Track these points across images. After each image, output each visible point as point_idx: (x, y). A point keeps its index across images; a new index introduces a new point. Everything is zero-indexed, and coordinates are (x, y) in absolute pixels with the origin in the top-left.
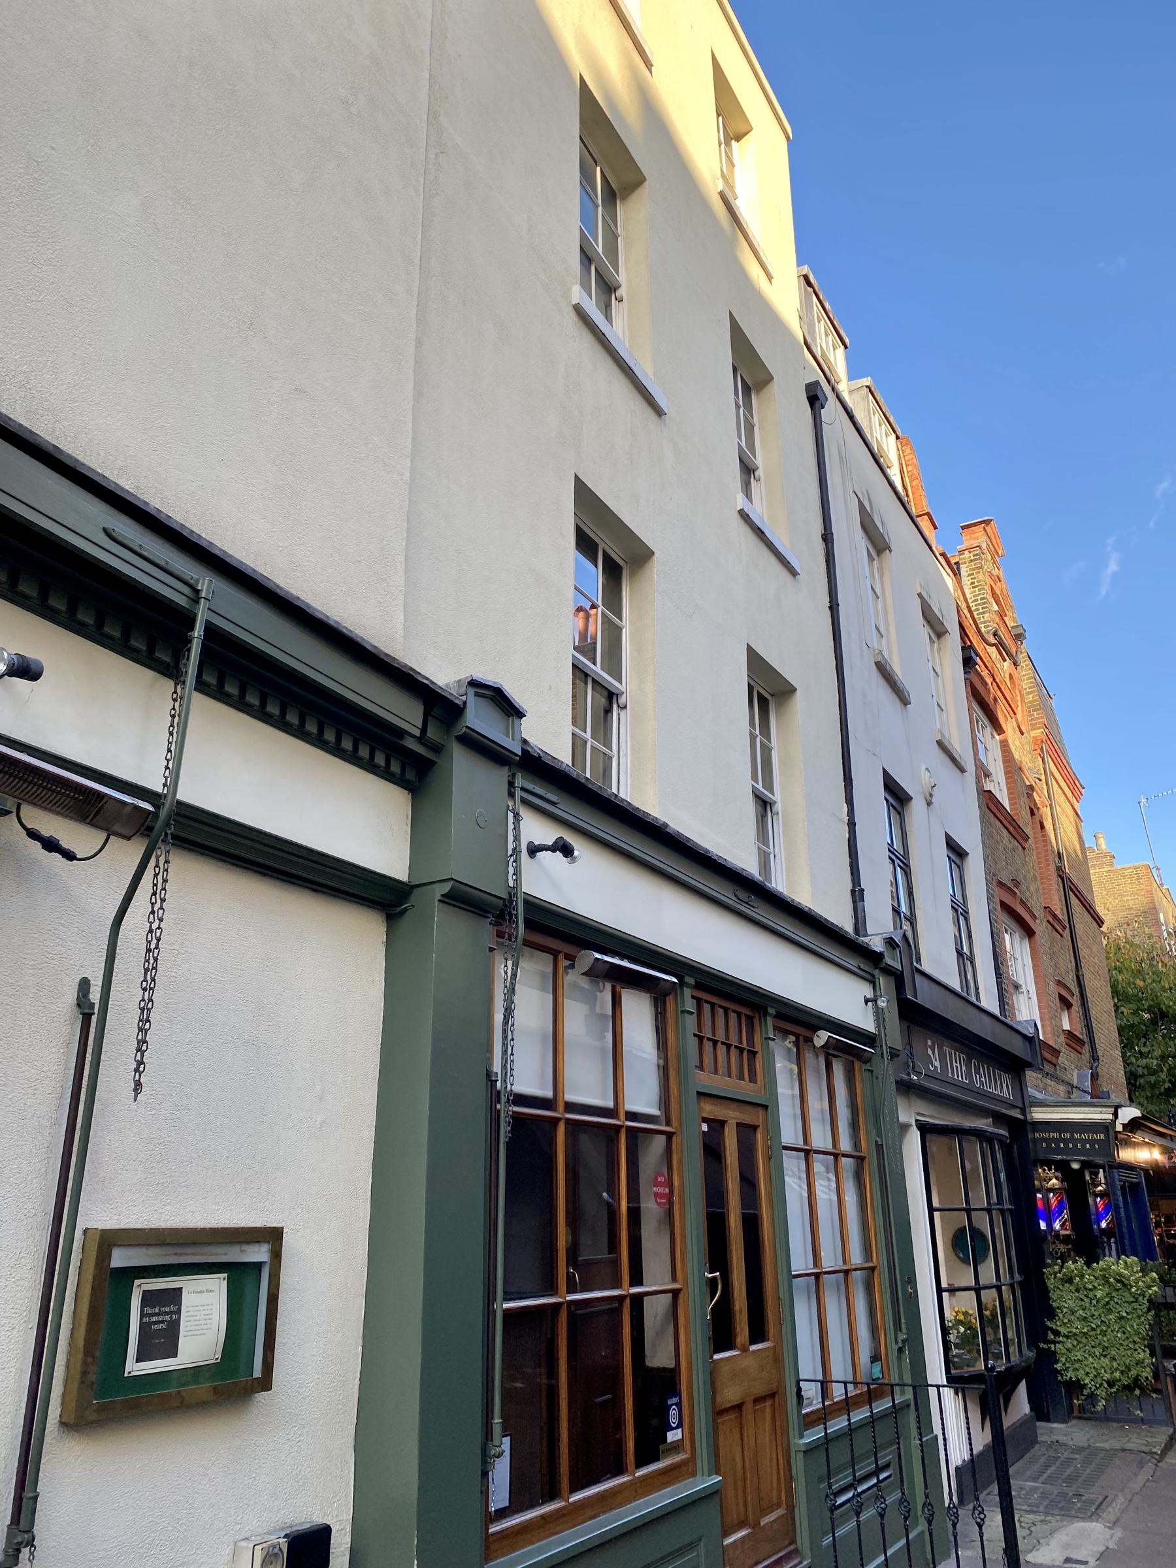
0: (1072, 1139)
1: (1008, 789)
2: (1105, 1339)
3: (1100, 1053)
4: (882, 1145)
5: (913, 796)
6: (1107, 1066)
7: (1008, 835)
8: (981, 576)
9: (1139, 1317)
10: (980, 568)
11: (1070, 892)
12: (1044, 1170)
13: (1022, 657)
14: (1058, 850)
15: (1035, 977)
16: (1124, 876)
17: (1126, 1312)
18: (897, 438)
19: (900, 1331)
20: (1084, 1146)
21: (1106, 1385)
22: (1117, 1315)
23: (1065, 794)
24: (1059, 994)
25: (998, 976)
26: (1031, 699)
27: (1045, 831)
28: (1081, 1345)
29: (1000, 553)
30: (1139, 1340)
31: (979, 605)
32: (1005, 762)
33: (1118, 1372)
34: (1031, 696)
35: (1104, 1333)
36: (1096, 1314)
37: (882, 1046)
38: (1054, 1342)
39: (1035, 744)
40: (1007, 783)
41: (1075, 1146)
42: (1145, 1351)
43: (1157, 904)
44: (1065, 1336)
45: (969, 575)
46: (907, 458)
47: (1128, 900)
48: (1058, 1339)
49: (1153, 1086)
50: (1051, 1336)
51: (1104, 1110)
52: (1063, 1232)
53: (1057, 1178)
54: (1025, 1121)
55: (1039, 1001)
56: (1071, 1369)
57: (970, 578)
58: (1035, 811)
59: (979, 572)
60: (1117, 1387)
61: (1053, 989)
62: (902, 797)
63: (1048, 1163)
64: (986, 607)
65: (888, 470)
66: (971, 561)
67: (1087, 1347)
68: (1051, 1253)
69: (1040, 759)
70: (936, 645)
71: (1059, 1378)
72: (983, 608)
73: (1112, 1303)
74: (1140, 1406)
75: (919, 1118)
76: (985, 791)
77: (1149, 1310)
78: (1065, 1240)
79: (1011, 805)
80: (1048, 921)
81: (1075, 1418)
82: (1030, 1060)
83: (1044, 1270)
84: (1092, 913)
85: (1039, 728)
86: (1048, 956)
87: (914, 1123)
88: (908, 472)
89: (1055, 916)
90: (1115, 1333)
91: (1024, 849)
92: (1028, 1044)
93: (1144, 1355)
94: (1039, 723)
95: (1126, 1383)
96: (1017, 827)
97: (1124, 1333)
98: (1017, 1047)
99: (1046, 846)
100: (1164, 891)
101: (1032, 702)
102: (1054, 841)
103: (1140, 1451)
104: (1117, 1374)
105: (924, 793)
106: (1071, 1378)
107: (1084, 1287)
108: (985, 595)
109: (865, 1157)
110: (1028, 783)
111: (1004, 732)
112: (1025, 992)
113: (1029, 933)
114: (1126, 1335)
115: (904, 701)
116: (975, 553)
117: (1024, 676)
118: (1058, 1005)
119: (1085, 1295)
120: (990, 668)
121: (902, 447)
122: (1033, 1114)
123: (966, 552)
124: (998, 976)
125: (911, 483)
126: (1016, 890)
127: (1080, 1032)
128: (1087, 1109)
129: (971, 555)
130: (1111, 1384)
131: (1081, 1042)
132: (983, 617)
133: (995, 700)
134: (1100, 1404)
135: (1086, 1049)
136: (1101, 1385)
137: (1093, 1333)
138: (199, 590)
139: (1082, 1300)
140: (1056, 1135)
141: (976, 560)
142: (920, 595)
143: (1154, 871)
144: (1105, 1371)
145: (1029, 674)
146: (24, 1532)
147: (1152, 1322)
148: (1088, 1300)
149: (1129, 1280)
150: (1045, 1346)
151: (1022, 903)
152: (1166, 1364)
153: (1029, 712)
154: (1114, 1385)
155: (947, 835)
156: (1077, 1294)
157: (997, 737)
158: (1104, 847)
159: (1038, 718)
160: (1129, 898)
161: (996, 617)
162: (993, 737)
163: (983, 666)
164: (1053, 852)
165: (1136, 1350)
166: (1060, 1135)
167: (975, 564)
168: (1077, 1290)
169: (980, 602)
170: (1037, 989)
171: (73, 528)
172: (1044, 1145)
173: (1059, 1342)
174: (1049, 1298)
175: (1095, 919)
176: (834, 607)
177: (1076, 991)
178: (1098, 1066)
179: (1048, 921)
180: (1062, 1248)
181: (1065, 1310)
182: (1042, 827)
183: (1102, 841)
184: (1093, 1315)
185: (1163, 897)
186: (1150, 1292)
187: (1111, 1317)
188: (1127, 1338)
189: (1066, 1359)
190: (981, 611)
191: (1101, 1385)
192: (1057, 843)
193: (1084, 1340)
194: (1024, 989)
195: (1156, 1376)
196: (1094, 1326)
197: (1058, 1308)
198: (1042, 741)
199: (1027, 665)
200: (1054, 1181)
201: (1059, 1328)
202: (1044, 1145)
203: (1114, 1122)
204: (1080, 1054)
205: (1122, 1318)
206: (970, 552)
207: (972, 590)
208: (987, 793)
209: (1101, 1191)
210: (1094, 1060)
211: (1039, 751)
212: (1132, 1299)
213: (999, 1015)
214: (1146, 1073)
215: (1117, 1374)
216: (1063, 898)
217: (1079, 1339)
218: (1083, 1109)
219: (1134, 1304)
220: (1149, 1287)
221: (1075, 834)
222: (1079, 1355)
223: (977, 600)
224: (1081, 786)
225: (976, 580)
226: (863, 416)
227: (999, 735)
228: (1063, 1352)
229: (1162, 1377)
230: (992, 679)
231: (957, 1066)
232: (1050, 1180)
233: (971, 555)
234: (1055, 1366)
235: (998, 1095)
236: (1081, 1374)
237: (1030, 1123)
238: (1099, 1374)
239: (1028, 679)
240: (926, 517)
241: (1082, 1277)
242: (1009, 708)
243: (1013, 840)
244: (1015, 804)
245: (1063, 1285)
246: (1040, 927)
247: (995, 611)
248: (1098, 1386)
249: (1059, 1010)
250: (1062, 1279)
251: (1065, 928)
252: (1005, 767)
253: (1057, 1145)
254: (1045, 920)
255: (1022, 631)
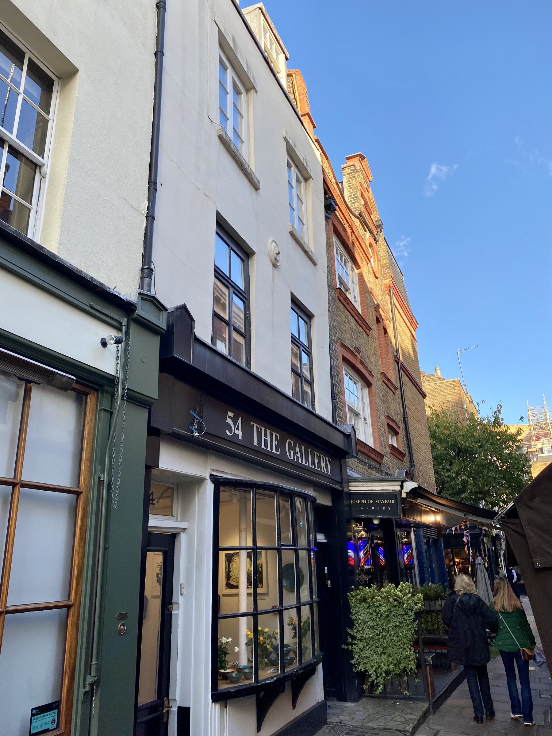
0: (374, 504)
1: (361, 301)
2: (385, 641)
3: (415, 463)
4: (103, 480)
5: (255, 251)
6: (422, 472)
7: (355, 322)
8: (354, 182)
9: (408, 625)
10: (353, 177)
11: (402, 371)
12: (357, 525)
13: (380, 238)
14: (396, 347)
15: (371, 411)
16: (447, 385)
17: (399, 622)
18: (287, 59)
19: (90, 674)
20: (381, 508)
21: (384, 675)
22: (393, 624)
23: (405, 322)
24: (388, 423)
25: (333, 398)
26: (385, 262)
27: (388, 334)
28: (369, 646)
29: (370, 179)
30: (407, 642)
31: (352, 198)
32: (360, 285)
33: (393, 664)
34: (384, 261)
35: (384, 637)
36: (380, 623)
37: (123, 389)
38: (352, 644)
39: (386, 287)
40: (361, 297)
41: (376, 508)
42: (411, 650)
43: (463, 400)
44: (358, 640)
45: (347, 182)
46: (298, 83)
47: (448, 398)
48: (354, 642)
49: (453, 488)
50: (350, 640)
51: (395, 483)
52: (366, 567)
53: (365, 531)
54: (342, 492)
55: (373, 425)
56: (362, 663)
57: (348, 183)
58: (381, 320)
59: (353, 180)
60: (391, 675)
61: (384, 421)
62: (248, 252)
63: (359, 520)
64: (356, 200)
65: (278, 74)
66: (349, 174)
67: (373, 647)
68: (358, 581)
69: (388, 297)
70: (303, 184)
71: (354, 670)
72: (354, 200)
73: (390, 615)
74: (408, 687)
75: (213, 473)
76: (337, 288)
77: (415, 620)
78: (368, 572)
79: (362, 310)
80: (383, 381)
81: (367, 696)
82: (346, 450)
83: (348, 594)
84: (419, 389)
85: (388, 279)
86: (381, 400)
87: (208, 477)
88: (298, 91)
89: (388, 380)
90: (392, 637)
91: (368, 335)
92: (346, 439)
93: (410, 652)
94: (389, 276)
95: (398, 672)
96: (362, 319)
97: (397, 636)
98: (338, 441)
99: (388, 345)
100: (468, 396)
101: (385, 264)
102: (394, 343)
103: (397, 730)
104: (392, 667)
105: (269, 255)
106: (361, 669)
107: (373, 604)
108: (356, 193)
109: (81, 493)
110: (376, 303)
111: (360, 268)
112: (363, 419)
113: (368, 384)
114: (399, 638)
115: (257, 188)
116: (351, 169)
117: (382, 249)
118: (387, 429)
119: (374, 611)
120: (350, 223)
121: (296, 76)
122: (350, 488)
123: (346, 169)
124: (333, 398)
125: (299, 96)
126: (357, 354)
127: (403, 448)
128: (384, 483)
129: (349, 170)
130: (387, 673)
131: (404, 455)
132: (354, 205)
133: (353, 244)
134: (379, 688)
135: (407, 459)
136: (381, 674)
137: (377, 637)
138: (122, 323)
139: (372, 614)
140: (364, 501)
141: (351, 173)
142: (285, 139)
143: (463, 387)
144: (384, 665)
145: (384, 248)
146: (93, 677)
147: (416, 629)
148: (376, 614)
149: (401, 599)
150: (346, 647)
151: (362, 363)
152: (426, 657)
153: (383, 269)
154: (390, 673)
155: (218, 215)
156: (368, 610)
157: (356, 271)
158: (439, 374)
159: (388, 273)
160: (449, 397)
161: (363, 207)
162: (353, 270)
163: (345, 220)
164: (393, 347)
165: (404, 649)
166: (367, 501)
167: (351, 175)
168: (369, 607)
169: (353, 196)
170: (372, 418)
171: (14, 265)
172: (357, 508)
173: (355, 644)
174: (350, 613)
175: (420, 393)
176: (159, 54)
177: (402, 426)
178: (414, 470)
179: (383, 381)
180: (366, 578)
181: (360, 621)
182: (385, 332)
183: (438, 371)
184: (378, 625)
185: (467, 398)
186: (416, 607)
187: (390, 626)
188: (400, 640)
189: (359, 656)
190: (353, 201)
191: (381, 674)
192: (396, 344)
193: (371, 643)
194: (362, 416)
195: (418, 666)
196: (378, 633)
197: (356, 620)
198: (390, 286)
199: (383, 244)
200: (363, 532)
201: (355, 634)
202: (357, 508)
203: (400, 491)
204: (403, 461)
205: (396, 626)
206: (348, 169)
207: (349, 190)
208: (338, 290)
209: (405, 541)
210: (412, 466)
211: (387, 292)
212: (403, 613)
213: (210, 343)
214: (449, 481)
215: (392, 667)
216: (398, 374)
217: (368, 641)
218: (381, 483)
219: (405, 616)
220: (416, 604)
221: (411, 345)
222: (367, 653)
223: (351, 196)
224: (417, 322)
225: (351, 185)
226: (255, 26)
227: (357, 269)
228: (357, 651)
229: (423, 667)
230: (351, 231)
231: (266, 441)
232: (360, 532)
233: (349, 170)
234: (351, 662)
235: (314, 469)
236: (368, 667)
237: (346, 493)
238: (379, 666)
239: (383, 251)
240: (307, 116)
241: (373, 597)
242: (365, 256)
243: (358, 327)
244: (365, 309)
245: (360, 604)
246: (377, 382)
247: (362, 204)
248: (379, 675)
249: (387, 433)
250: (360, 600)
251: (396, 389)
252: (360, 288)
253: (365, 508)
254: (381, 380)
255: (380, 223)
